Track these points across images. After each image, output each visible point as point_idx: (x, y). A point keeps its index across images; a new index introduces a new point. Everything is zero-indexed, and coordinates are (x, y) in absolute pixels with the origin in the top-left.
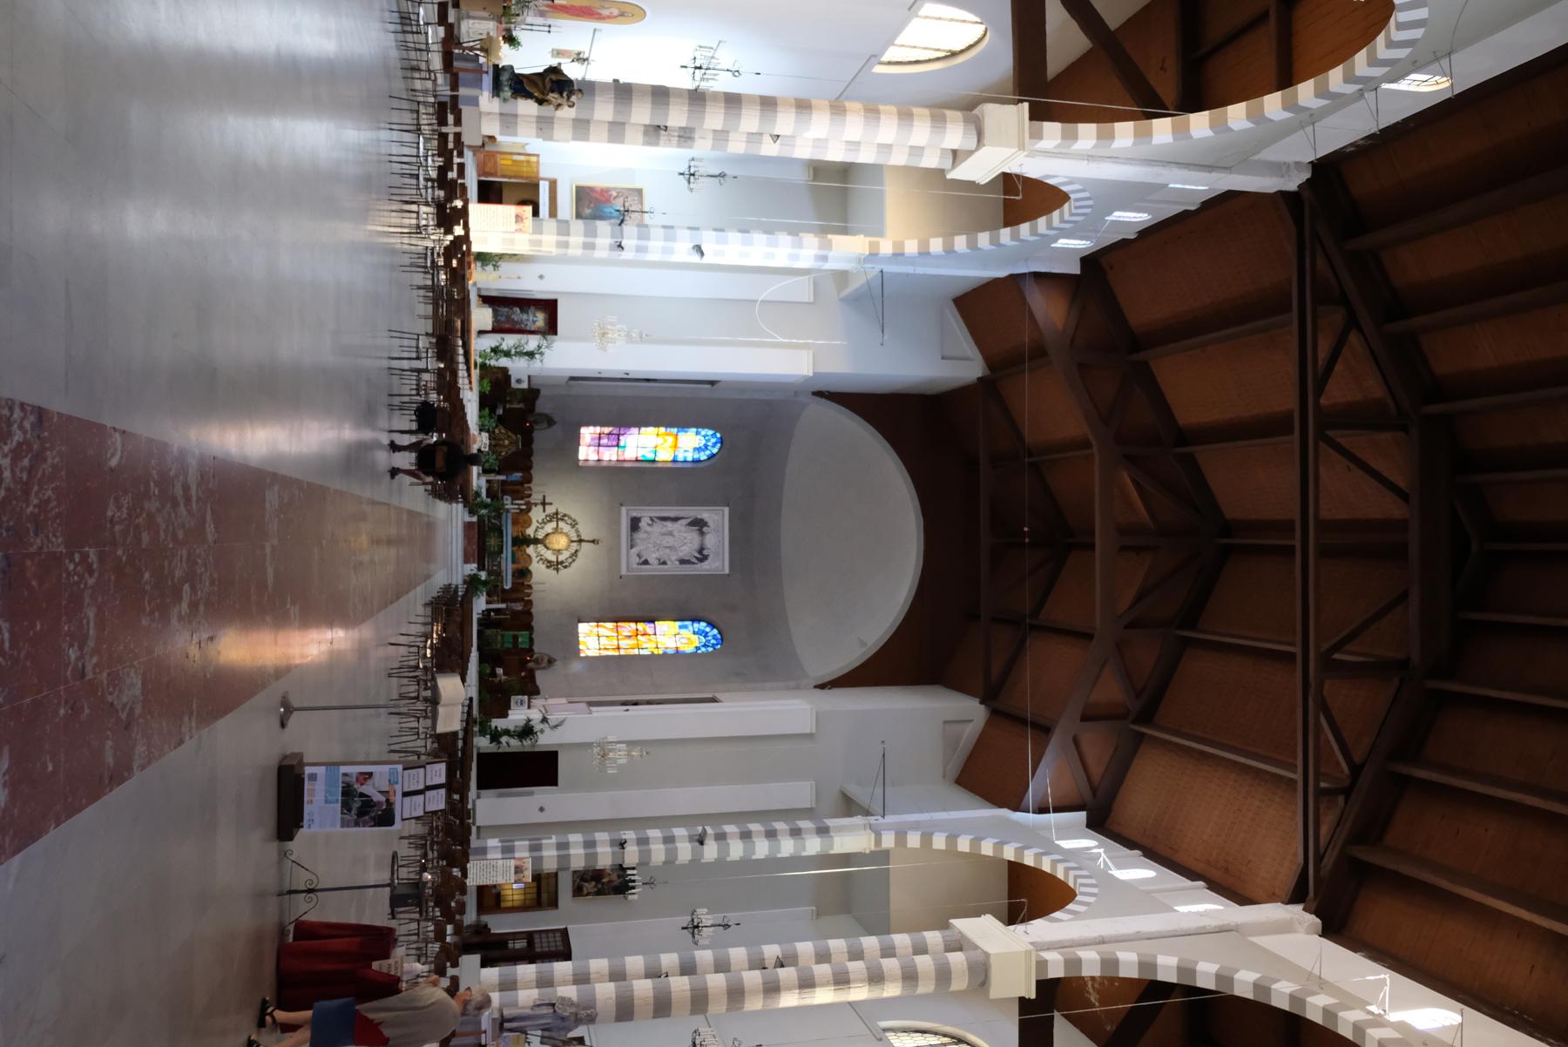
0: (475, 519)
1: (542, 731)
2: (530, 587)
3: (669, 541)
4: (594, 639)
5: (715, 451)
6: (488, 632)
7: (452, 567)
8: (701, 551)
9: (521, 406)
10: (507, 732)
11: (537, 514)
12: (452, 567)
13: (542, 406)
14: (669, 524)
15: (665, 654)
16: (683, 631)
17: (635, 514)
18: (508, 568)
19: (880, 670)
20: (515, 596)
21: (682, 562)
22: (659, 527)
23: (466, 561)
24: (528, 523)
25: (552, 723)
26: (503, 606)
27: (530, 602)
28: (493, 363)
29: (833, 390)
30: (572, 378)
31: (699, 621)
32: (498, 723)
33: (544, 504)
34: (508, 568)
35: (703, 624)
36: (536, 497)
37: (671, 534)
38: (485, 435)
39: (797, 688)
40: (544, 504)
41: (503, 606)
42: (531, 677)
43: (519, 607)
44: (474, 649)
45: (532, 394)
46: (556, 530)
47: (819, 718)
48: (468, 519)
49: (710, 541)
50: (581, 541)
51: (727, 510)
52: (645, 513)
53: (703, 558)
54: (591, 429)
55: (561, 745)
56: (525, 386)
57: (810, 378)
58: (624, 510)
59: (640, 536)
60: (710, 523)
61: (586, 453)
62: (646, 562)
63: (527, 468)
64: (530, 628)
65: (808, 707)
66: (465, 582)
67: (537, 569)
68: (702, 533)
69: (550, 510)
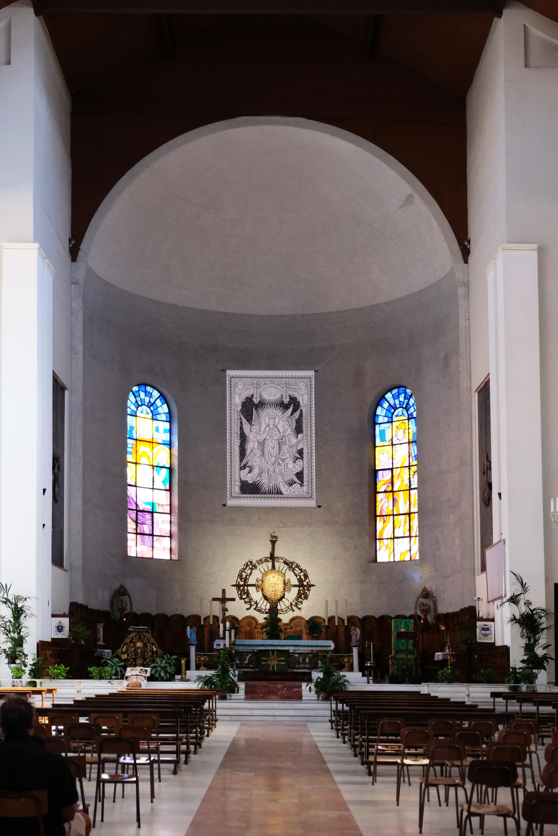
0: (242, 686)
1: (528, 603)
2: (331, 619)
3: (271, 446)
4: (397, 544)
5: (156, 394)
6: (392, 670)
7: (307, 717)
8: (284, 406)
9: (100, 627)
10: (529, 648)
11: (238, 609)
12: (307, 717)
13: (99, 601)
14: (249, 446)
15: (417, 457)
16: (388, 437)
17: (237, 489)
18: (307, 644)
19: (448, 183)
20: (342, 637)
21: (299, 429)
22: (254, 459)
23: (298, 697)
24: (251, 620)
25: (518, 589)
26: (355, 651)
27: (350, 618)
28: (30, 660)
29: (67, 234)
30: (58, 559)
31: (375, 416)
32: (517, 659)
33: (224, 600)
34: (307, 644)
35: (379, 411)
36: (216, 609)
37: (262, 444)
38: (129, 672)
39: (467, 285)
40: (224, 600)
41: (355, 651)
42: (448, 618)
43: (357, 633)
44: (424, 688)
45: (77, 613)
46: (259, 587)
47: (517, 239)
48: (242, 694)
49: (271, 394)
50: (272, 557)
51: (229, 373)
52: (235, 475)
53: (294, 403)
54: (131, 543)
55: (547, 580)
56: (65, 622)
57: (41, 245)
58: (231, 502)
59: (265, 482)
60: (248, 394)
61: (162, 550)
62: (300, 475)
63: (182, 621)
64: (384, 620)
65: (500, 256)
66: (326, 699)
67: (308, 610)
68: (262, 404)
69: (232, 593)
